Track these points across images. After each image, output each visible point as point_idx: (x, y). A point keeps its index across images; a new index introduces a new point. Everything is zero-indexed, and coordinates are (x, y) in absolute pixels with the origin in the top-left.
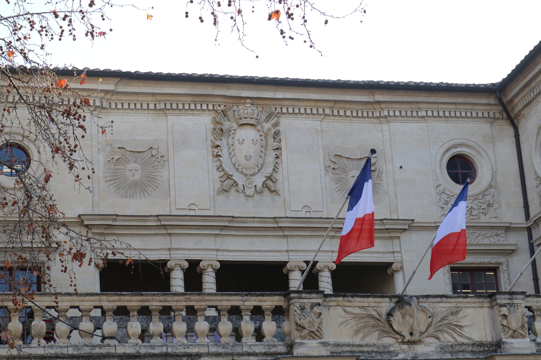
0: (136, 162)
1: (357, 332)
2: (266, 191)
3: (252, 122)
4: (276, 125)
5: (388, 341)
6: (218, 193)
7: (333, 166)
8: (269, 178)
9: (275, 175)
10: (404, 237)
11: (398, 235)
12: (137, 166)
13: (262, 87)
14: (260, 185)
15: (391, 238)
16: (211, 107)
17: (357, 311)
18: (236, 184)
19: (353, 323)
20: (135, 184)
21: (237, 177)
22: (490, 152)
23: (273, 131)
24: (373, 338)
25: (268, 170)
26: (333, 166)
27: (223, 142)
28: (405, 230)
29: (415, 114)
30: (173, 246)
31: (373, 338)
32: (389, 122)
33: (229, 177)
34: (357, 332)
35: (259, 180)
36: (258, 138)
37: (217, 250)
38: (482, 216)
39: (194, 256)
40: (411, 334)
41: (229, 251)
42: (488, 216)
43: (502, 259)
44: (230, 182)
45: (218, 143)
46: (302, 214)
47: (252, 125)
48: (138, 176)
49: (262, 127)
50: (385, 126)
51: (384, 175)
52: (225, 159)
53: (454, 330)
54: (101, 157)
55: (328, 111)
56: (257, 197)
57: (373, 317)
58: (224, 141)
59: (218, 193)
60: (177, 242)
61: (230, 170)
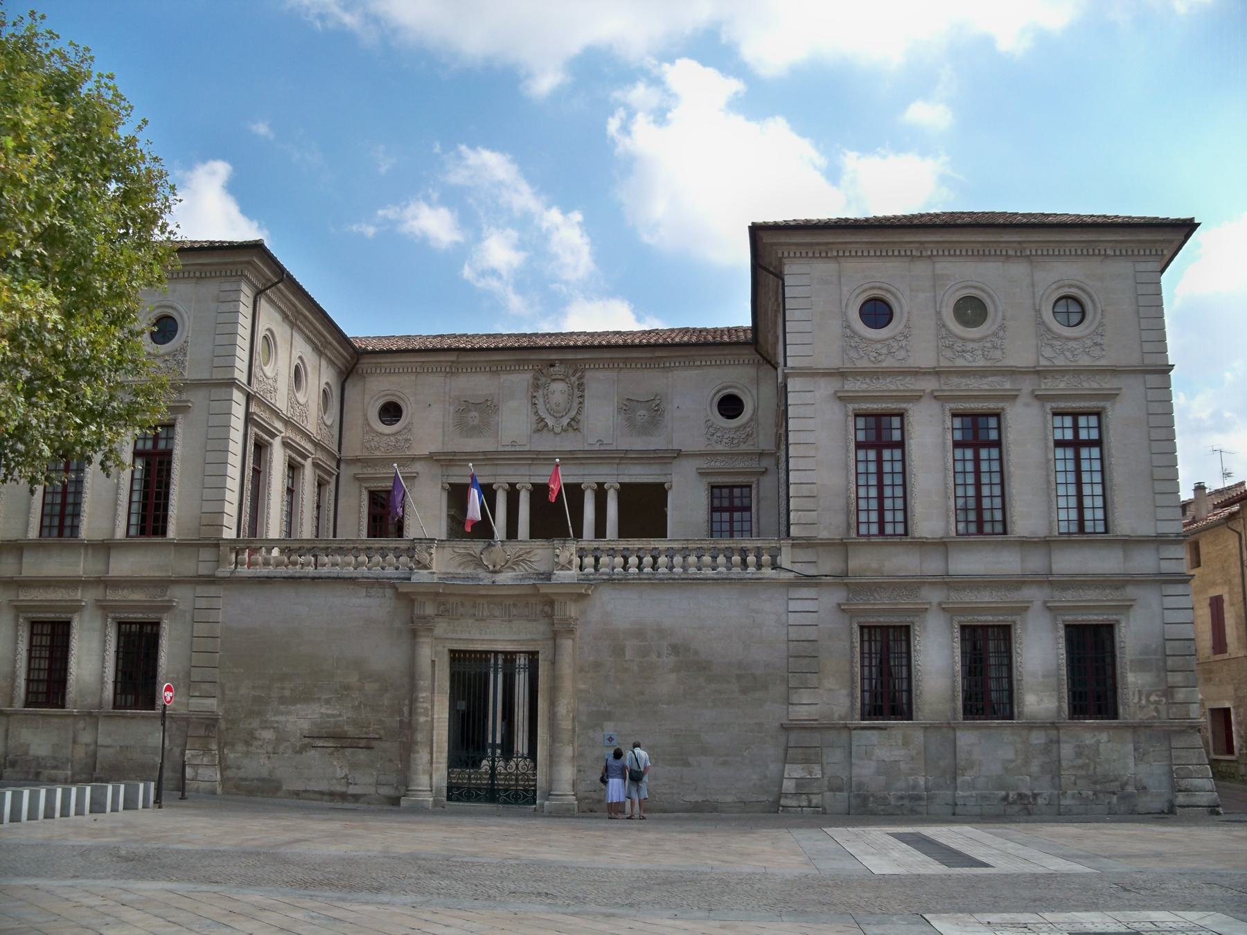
0: (476, 411)
1: (460, 565)
2: (570, 429)
3: (561, 377)
4: (580, 378)
5: (480, 570)
6: (535, 432)
7: (625, 408)
8: (573, 419)
9: (579, 417)
10: (676, 462)
11: (670, 461)
12: (476, 414)
13: (989, 230)
14: (565, 424)
15: (666, 463)
16: (531, 367)
17: (462, 551)
18: (546, 425)
19: (458, 559)
20: (474, 428)
21: (550, 421)
22: (754, 392)
23: (577, 383)
24: (469, 571)
25: (573, 413)
26: (625, 408)
27: (540, 394)
28: (675, 457)
29: (692, 364)
30: (498, 473)
31: (469, 571)
32: (672, 371)
33: (542, 420)
34: (460, 565)
35: (565, 421)
36: (566, 389)
37: (530, 476)
38: (742, 444)
39: (513, 480)
40: (494, 566)
41: (539, 476)
42: (747, 444)
43: (754, 479)
44: (542, 424)
45: (535, 394)
46: (596, 448)
47: (563, 380)
48: (476, 422)
49: (570, 380)
50: (670, 374)
51: (666, 413)
52: (541, 406)
53: (526, 564)
54: (452, 408)
55: (621, 365)
56: (563, 434)
57: (471, 555)
58: (541, 392)
59: (535, 432)
60: (501, 470)
61: (543, 414)
